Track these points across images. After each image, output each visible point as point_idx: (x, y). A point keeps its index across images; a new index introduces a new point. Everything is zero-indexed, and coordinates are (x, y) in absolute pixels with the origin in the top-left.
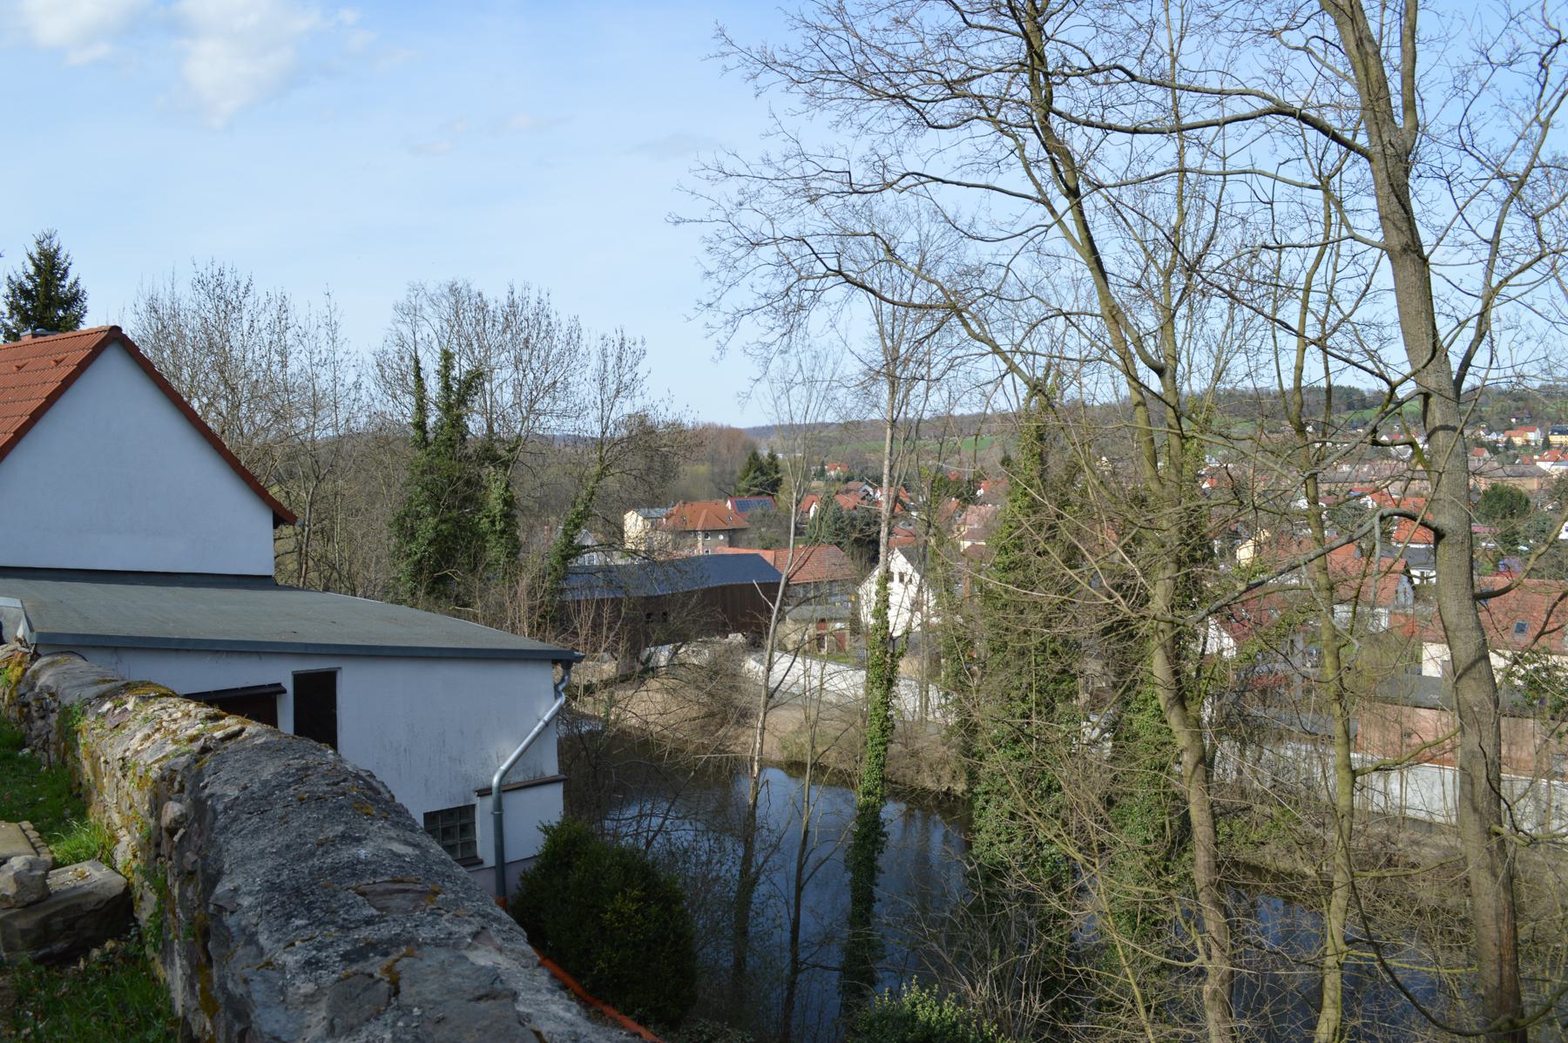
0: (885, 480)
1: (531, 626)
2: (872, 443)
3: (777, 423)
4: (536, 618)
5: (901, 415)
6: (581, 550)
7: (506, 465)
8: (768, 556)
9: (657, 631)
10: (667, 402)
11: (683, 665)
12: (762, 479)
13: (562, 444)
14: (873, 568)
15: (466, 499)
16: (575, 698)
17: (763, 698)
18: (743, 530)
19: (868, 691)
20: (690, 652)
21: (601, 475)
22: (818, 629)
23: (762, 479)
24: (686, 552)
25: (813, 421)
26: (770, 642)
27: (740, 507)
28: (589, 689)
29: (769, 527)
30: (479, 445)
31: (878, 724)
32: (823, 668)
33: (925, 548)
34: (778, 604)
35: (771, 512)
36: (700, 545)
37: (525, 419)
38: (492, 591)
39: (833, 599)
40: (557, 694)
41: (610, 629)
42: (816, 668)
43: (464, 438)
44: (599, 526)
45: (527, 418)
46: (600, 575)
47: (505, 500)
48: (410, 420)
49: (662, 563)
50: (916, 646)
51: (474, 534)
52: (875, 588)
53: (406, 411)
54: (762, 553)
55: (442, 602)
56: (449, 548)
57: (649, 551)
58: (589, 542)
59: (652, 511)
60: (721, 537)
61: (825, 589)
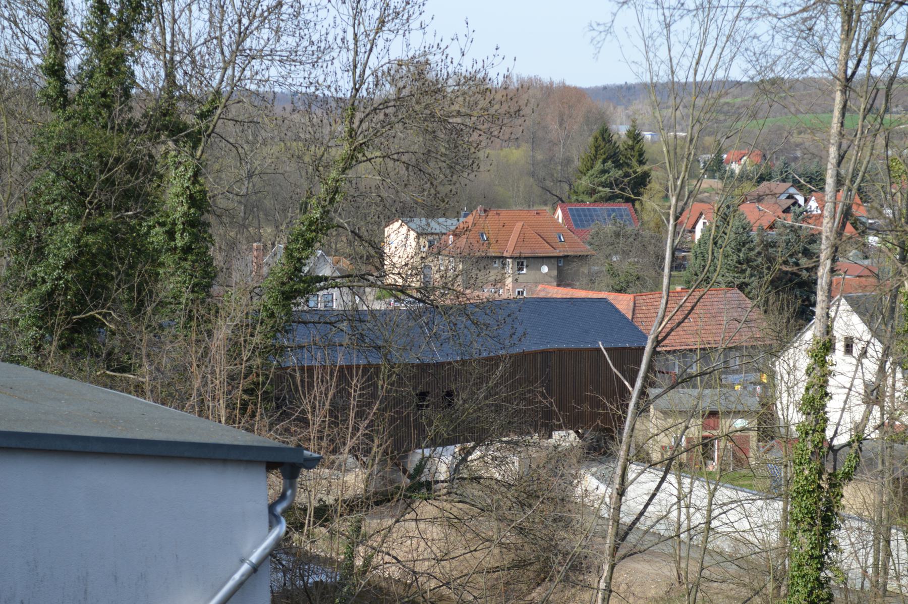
0: (830, 181)
1: (230, 406)
2: (809, 116)
3: (647, 79)
4: (239, 393)
5: (862, 71)
6: (314, 283)
7: (195, 139)
8: (623, 303)
9: (438, 424)
10: (463, 40)
11: (477, 479)
12: (617, 173)
13: (289, 108)
14: (800, 329)
15: (128, 195)
16: (299, 527)
17: (609, 541)
18: (581, 258)
19: (788, 535)
20: (488, 460)
21: (350, 161)
22: (705, 427)
23: (617, 173)
24: (487, 293)
25: (708, 78)
26: (624, 447)
27: (578, 220)
28: (323, 514)
29: (626, 254)
30: (152, 104)
31: (804, 591)
32: (712, 494)
33: (895, 297)
34: (639, 383)
35: (629, 229)
36: (509, 281)
37: (228, 63)
38: (169, 347)
39: (731, 378)
40: (273, 519)
41: (360, 415)
42: (699, 494)
43: (127, 94)
44: (342, 244)
45: (232, 62)
46: (344, 325)
47: (191, 197)
48: (38, 61)
49: (447, 310)
50: (871, 463)
51: (140, 252)
52: (804, 362)
53: (32, 46)
54: (612, 297)
55: (87, 361)
56: (98, 275)
57: (426, 288)
58: (326, 271)
59: (433, 224)
60: (545, 269)
61: (716, 361)
